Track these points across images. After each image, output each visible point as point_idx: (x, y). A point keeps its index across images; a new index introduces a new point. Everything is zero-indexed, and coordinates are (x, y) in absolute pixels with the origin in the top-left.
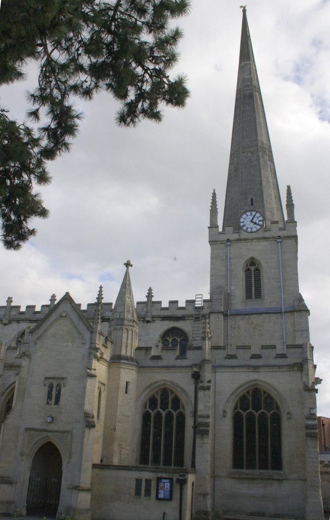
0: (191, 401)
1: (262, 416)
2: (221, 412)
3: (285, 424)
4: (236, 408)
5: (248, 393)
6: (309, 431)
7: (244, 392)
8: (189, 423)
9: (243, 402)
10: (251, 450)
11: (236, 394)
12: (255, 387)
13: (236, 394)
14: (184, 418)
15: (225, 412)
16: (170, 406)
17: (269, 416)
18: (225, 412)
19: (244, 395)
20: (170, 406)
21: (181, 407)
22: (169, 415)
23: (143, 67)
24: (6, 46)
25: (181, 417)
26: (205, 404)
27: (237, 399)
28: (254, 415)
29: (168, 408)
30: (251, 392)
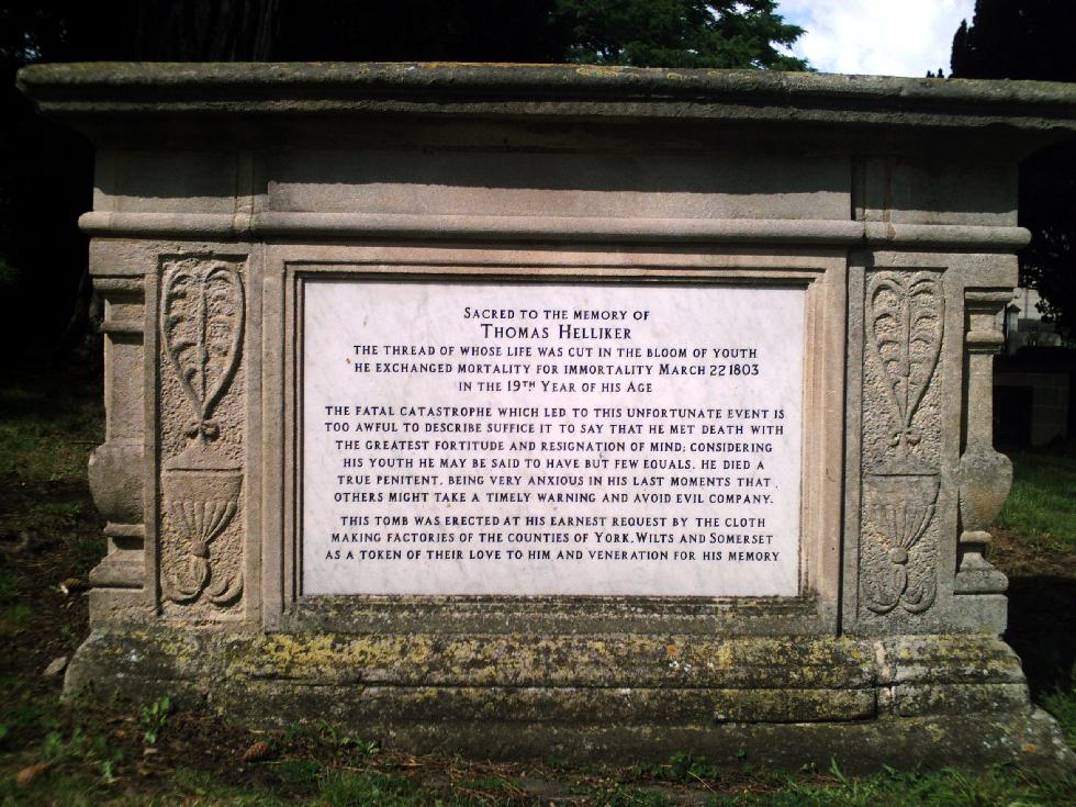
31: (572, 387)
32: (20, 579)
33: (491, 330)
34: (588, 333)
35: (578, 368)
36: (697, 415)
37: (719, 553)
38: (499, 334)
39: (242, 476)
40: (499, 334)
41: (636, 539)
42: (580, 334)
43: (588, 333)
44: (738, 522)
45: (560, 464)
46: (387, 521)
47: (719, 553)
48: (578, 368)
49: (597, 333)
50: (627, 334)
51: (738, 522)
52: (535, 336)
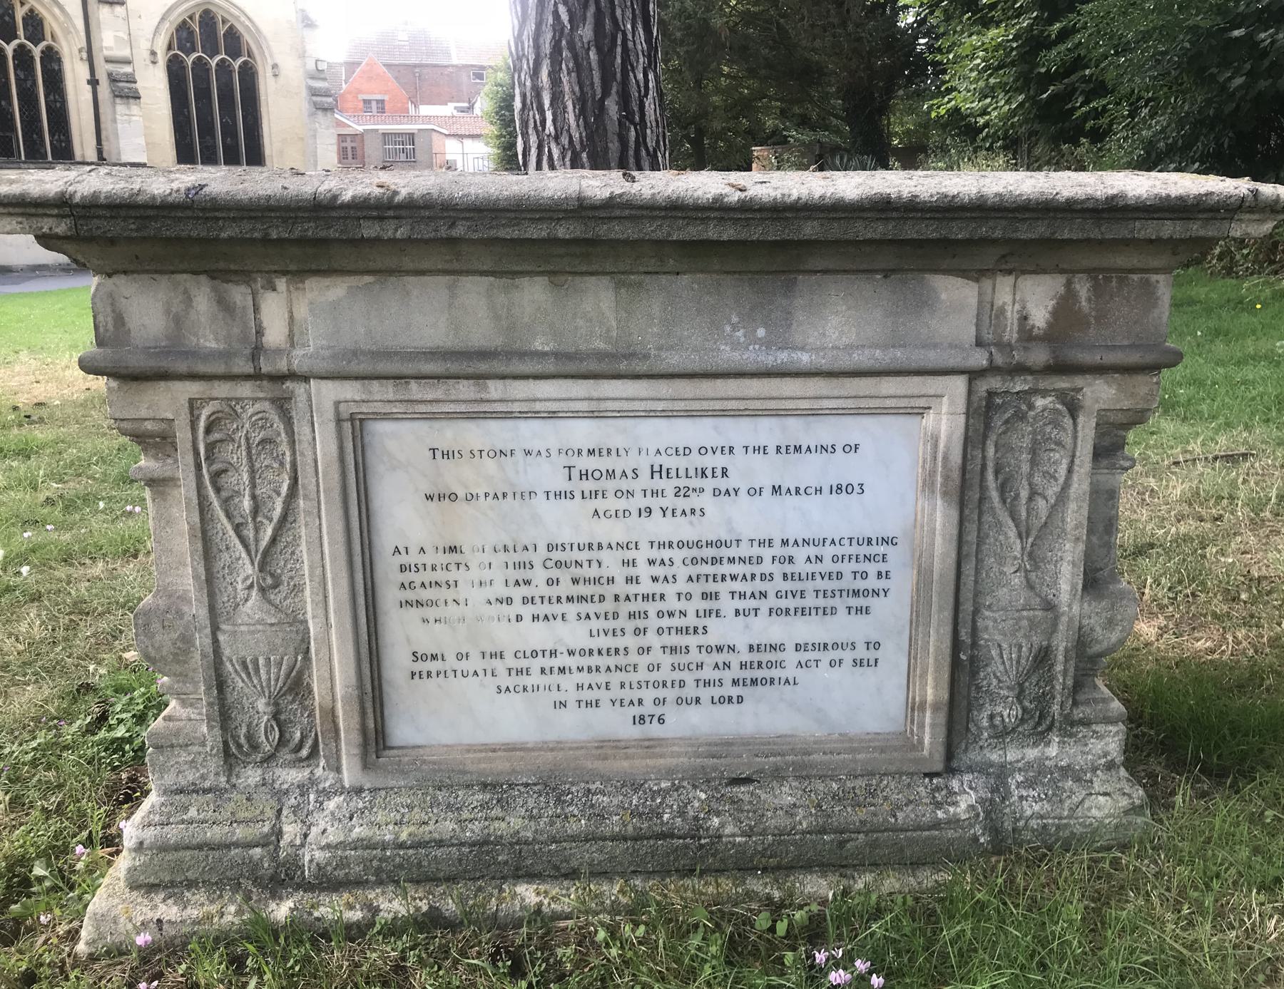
0: (75, 27)
1: (199, 62)
2: (146, 55)
3: (269, 90)
4: (170, 48)
5: (191, 18)
6: (318, 99)
7: (185, 16)
8: (75, 75)
9: (183, 36)
10: (207, 129)
11: (171, 18)
12: (204, 8)
13: (171, 18)
14: (59, 61)
15: (153, 53)
16: (21, 32)
17: (236, 67)
18: (153, 53)
19: (184, 22)
20: (21, 32)
21: (48, 36)
22: (22, 53)
23: (229, 777)
24: (608, 929)
25: (52, 58)
26: (117, 34)
27: (173, 29)
28: (182, 61)
29: (16, 37)
30: (197, 16)
31: (698, 701)
32: (32, 623)
33: (575, 473)
34: (682, 473)
35: (737, 560)
36: (726, 647)
37: (686, 647)
38: (584, 477)
39: (110, 75)
40: (584, 477)
41: (566, 653)
42: (673, 473)
43: (682, 473)
44: (528, 654)
45: (590, 686)
46: (709, 650)
47: (686, 647)
48: (737, 560)
49: (692, 473)
50: (724, 472)
51: (528, 654)
52: (624, 478)
